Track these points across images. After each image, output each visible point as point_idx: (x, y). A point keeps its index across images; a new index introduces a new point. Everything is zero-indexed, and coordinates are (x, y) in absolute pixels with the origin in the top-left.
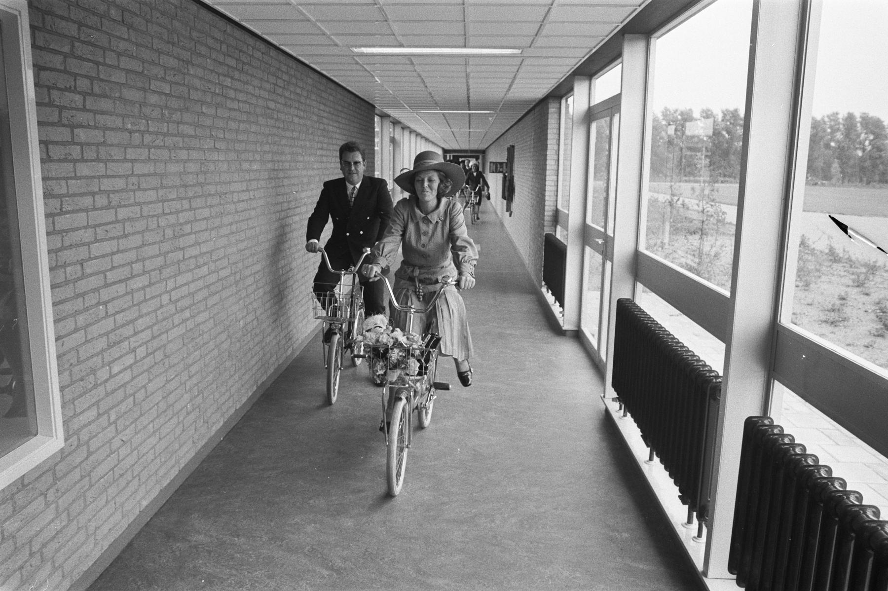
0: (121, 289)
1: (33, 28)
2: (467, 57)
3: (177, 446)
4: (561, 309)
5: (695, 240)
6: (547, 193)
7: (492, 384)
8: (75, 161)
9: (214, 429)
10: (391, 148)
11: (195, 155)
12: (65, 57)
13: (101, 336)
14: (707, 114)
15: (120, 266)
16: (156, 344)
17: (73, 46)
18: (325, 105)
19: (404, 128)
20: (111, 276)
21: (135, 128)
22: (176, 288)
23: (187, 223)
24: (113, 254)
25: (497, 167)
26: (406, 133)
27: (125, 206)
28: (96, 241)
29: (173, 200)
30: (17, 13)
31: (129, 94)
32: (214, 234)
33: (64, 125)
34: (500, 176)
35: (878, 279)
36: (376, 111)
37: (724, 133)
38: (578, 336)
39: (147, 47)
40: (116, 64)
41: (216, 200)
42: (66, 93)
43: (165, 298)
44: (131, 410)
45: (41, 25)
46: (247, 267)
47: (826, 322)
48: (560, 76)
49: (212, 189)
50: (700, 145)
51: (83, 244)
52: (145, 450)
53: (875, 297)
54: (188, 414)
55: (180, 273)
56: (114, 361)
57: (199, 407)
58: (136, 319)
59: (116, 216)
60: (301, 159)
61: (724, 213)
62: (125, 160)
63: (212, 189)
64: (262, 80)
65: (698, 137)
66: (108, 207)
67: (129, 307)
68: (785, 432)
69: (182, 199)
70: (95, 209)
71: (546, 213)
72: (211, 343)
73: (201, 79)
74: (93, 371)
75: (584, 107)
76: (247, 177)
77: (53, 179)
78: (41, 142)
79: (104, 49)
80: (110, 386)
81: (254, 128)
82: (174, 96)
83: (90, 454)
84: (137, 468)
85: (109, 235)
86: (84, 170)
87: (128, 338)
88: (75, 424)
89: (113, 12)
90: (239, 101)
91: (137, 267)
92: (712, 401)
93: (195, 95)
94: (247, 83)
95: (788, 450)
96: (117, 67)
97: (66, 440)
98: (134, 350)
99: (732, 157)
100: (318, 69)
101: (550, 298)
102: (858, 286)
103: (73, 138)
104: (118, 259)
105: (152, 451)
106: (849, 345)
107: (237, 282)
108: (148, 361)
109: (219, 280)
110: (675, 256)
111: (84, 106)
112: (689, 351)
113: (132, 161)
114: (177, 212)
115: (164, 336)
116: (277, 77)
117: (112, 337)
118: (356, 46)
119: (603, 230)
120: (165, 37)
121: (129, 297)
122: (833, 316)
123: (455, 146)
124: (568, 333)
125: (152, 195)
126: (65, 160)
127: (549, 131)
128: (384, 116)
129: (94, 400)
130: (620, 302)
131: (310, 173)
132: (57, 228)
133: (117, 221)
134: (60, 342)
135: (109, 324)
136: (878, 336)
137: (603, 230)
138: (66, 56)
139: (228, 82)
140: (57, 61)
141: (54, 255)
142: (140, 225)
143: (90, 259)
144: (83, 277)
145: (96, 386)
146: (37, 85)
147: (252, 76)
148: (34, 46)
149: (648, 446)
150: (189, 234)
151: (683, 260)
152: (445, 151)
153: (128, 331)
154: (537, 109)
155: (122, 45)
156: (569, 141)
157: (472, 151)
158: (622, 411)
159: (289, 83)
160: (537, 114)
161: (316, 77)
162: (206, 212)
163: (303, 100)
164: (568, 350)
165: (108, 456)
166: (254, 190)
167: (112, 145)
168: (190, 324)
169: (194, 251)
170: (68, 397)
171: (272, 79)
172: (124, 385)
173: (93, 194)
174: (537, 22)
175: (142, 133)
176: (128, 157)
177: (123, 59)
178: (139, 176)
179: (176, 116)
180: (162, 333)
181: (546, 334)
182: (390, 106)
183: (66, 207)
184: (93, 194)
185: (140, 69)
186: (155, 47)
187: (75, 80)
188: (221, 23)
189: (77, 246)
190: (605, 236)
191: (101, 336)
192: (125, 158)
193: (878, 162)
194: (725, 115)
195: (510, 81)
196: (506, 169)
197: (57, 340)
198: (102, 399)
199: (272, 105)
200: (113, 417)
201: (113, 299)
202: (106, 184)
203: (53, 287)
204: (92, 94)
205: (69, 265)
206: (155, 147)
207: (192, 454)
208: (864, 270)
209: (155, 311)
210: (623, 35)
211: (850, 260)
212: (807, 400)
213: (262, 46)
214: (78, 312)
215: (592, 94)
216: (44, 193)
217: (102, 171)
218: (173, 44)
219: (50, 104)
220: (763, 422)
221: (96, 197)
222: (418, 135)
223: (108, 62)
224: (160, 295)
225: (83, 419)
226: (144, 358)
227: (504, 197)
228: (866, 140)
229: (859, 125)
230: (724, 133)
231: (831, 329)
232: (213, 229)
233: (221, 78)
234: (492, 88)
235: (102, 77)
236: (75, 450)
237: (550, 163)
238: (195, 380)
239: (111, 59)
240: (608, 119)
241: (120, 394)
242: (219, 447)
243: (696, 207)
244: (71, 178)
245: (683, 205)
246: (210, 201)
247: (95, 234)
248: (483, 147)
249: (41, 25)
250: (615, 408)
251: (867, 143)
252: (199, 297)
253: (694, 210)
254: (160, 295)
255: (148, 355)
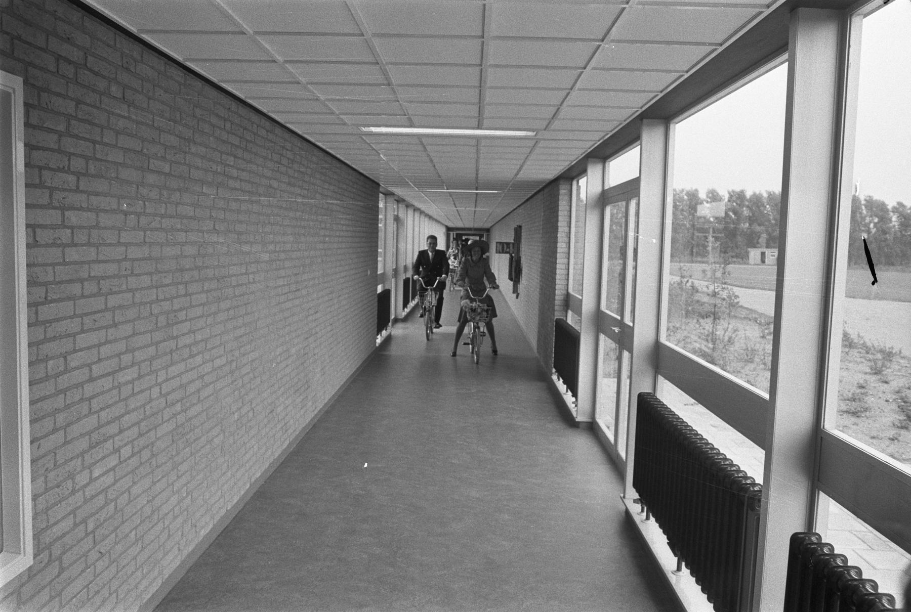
0: (107, 383)
1: (27, 105)
2: (478, 138)
3: (160, 555)
4: (574, 399)
5: (707, 324)
6: (558, 277)
7: (504, 482)
8: (64, 246)
9: (203, 533)
10: (395, 226)
11: (192, 237)
12: (60, 136)
13: (82, 435)
14: (714, 197)
15: (108, 358)
16: (142, 442)
17: (69, 124)
18: (330, 184)
19: (408, 206)
20: (97, 370)
21: (131, 209)
22: (167, 380)
23: (181, 309)
24: (100, 345)
25: (503, 248)
26: (410, 212)
27: (115, 293)
28: (83, 331)
29: (167, 285)
30: (11, 91)
31: (125, 174)
32: (210, 320)
33: (55, 208)
34: (508, 256)
35: (895, 366)
36: (381, 190)
37: (731, 214)
38: (592, 428)
39: (147, 125)
40: (114, 143)
41: (214, 285)
42: (60, 174)
43: (155, 392)
44: (111, 517)
45: (36, 103)
46: (244, 355)
47: (847, 412)
48: (572, 158)
49: (210, 273)
50: (706, 226)
51: (69, 335)
52: (125, 562)
53: (895, 384)
54: (175, 517)
55: (172, 364)
56: (95, 464)
57: (187, 510)
58: (123, 416)
59: (106, 304)
60: (303, 239)
61: (736, 297)
62: (119, 243)
63: (210, 273)
64: (265, 158)
65: (705, 218)
66: (98, 294)
67: (116, 403)
68: (836, 552)
69: (178, 284)
70: (83, 296)
71: (557, 298)
72: (202, 439)
73: (203, 157)
74: (71, 476)
75: (596, 189)
76: (247, 260)
77: (38, 265)
78: (28, 226)
79: (102, 127)
80: (89, 492)
81: (256, 208)
82: (175, 176)
83: (62, 570)
84: (115, 584)
85: (97, 325)
86: (73, 254)
87: (112, 437)
88: (46, 539)
89: (114, 88)
90: (241, 180)
91: (127, 359)
92: (749, 511)
93: (196, 174)
94: (250, 162)
95: (828, 561)
96: (115, 146)
97: (35, 556)
98: (117, 450)
99: (739, 238)
100: (324, 147)
101: (561, 386)
102: (876, 373)
103: (63, 221)
104: (105, 350)
105: (133, 563)
106: (873, 438)
107: (232, 372)
108: (134, 462)
109: (214, 369)
110: (686, 342)
111: (78, 187)
112: (708, 444)
113: (127, 245)
114: (171, 299)
115: (152, 434)
116: (282, 155)
117: (95, 436)
118: (365, 126)
119: (619, 318)
120: (167, 115)
121: (115, 392)
122: (853, 406)
123: (460, 225)
124: (581, 426)
125: (146, 281)
126: (54, 245)
127: (560, 213)
128: (388, 194)
129: (70, 508)
130: (640, 396)
131: (312, 253)
132: (41, 318)
133: (107, 309)
134: (36, 444)
135: (92, 421)
136: (902, 428)
137: (619, 318)
138: (60, 135)
139: (231, 160)
140: (51, 140)
141: (34, 309)
142: (131, 313)
143: (75, 351)
144: (66, 371)
145: (73, 492)
146: (27, 165)
147: (256, 154)
148: (27, 124)
149: (675, 555)
150: (182, 322)
151: (697, 345)
152: (449, 229)
153: (113, 429)
154: (546, 190)
155: (121, 123)
156: (581, 224)
157: (476, 229)
158: (645, 514)
159: (293, 161)
160: (547, 196)
161: (321, 154)
162: (203, 298)
163: (307, 178)
164: (581, 444)
165: (83, 571)
166: (253, 273)
167: (105, 228)
168: (181, 419)
169: (187, 340)
170: (40, 507)
171: (276, 157)
172: (105, 490)
173: (82, 281)
174: (554, 106)
175: (138, 215)
176: (122, 240)
177: (121, 137)
178: (133, 260)
179: (176, 196)
180: (150, 430)
181: (558, 425)
182: (396, 184)
183: (51, 296)
184: (82, 281)
185: (139, 149)
186: (156, 125)
187: (69, 160)
188: (227, 101)
189: (61, 337)
190: (621, 323)
191: (82, 435)
192: (119, 242)
193: (883, 244)
194: (731, 196)
195: (521, 162)
196: (513, 250)
197: (32, 442)
198: (80, 507)
199: (275, 184)
200: (91, 526)
201: (98, 395)
202: (97, 270)
203: (31, 384)
204: (86, 174)
205: (52, 358)
206: (151, 230)
207: (178, 563)
208: (879, 356)
209: (144, 406)
210: (642, 120)
211: (864, 345)
212: (858, 517)
213: (268, 124)
214: (58, 411)
215: (606, 176)
216: (28, 281)
217: (93, 256)
218: (175, 122)
219: (41, 185)
220: (810, 539)
221: (86, 283)
222: (422, 212)
223: (105, 140)
224: (150, 388)
225: (57, 530)
226: (129, 458)
227: (511, 279)
228: (870, 222)
229: (863, 207)
230: (731, 214)
231: (853, 419)
232: (209, 315)
233: (224, 157)
234: (502, 169)
235: (98, 156)
236: (45, 567)
237: (561, 246)
238: (184, 480)
239: (109, 137)
240: (624, 203)
241: (101, 500)
242: (207, 554)
243: (705, 289)
244: (58, 264)
245: (692, 287)
246: (207, 286)
247: (82, 324)
248: (487, 226)
249: (36, 103)
250: (636, 510)
251: (872, 225)
252: (192, 389)
253: (703, 293)
254: (150, 388)
255: (133, 455)
